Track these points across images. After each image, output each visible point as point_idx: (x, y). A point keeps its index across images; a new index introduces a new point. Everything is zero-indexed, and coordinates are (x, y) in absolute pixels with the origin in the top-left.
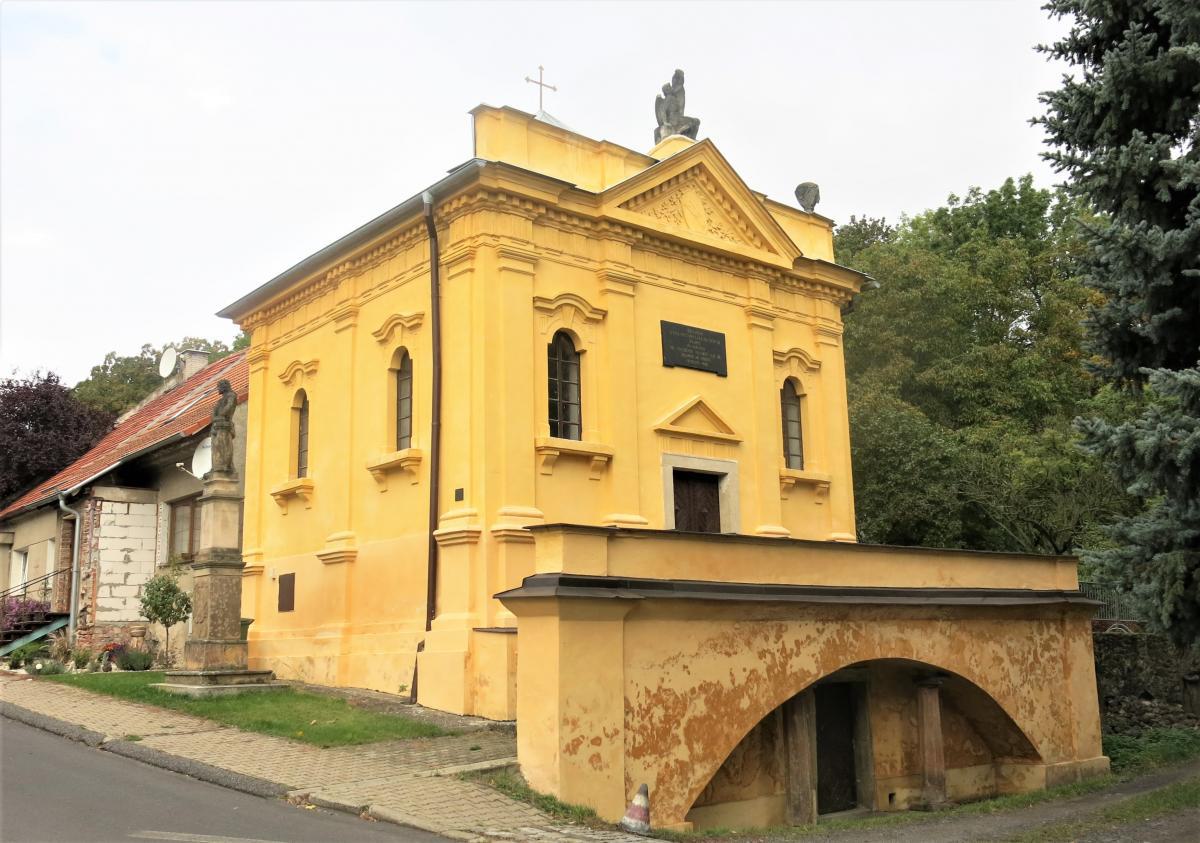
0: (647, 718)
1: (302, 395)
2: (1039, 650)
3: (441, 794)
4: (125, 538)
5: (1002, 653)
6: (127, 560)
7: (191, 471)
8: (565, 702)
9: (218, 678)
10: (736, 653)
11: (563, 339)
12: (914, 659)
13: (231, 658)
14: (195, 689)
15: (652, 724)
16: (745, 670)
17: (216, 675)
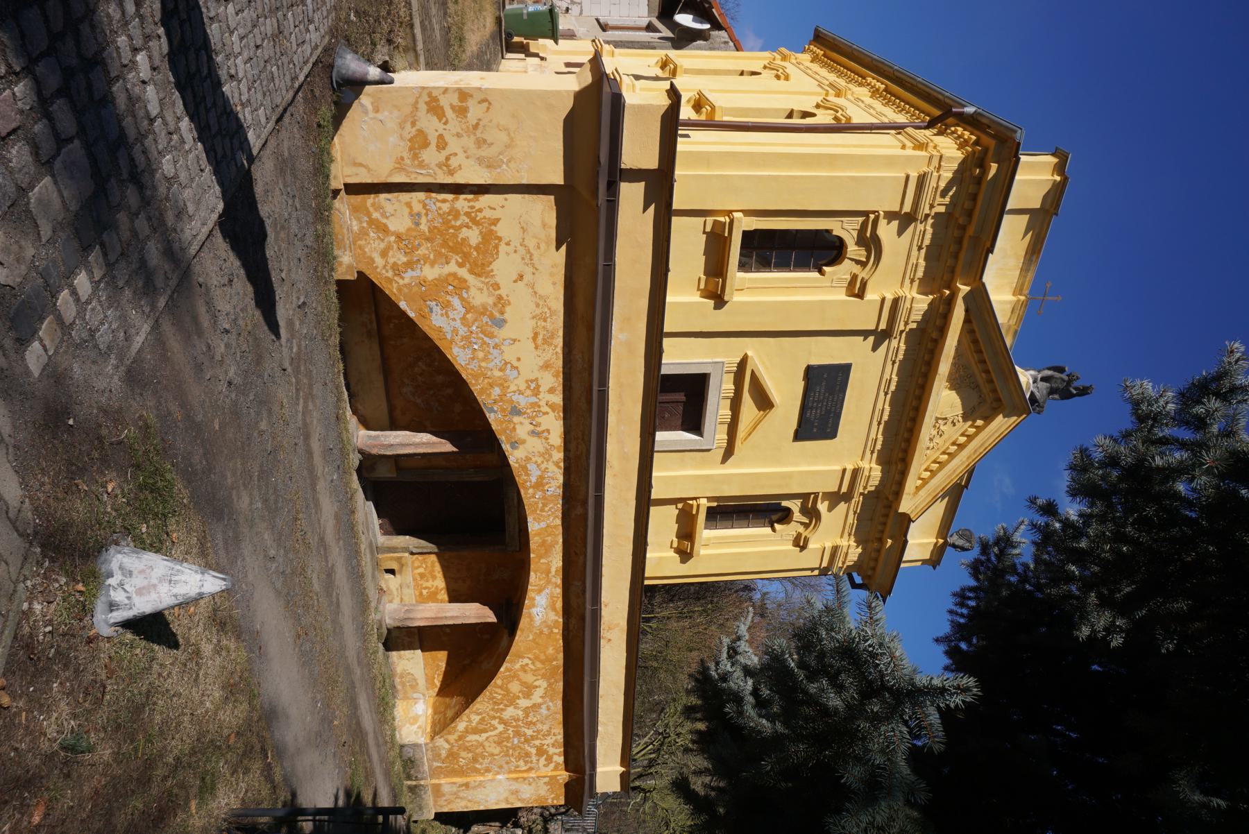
0: (467, 220)
2: (537, 742)
5: (537, 698)
7: (679, 13)
10: (536, 348)
11: (835, 252)
12: (530, 587)
15: (461, 227)
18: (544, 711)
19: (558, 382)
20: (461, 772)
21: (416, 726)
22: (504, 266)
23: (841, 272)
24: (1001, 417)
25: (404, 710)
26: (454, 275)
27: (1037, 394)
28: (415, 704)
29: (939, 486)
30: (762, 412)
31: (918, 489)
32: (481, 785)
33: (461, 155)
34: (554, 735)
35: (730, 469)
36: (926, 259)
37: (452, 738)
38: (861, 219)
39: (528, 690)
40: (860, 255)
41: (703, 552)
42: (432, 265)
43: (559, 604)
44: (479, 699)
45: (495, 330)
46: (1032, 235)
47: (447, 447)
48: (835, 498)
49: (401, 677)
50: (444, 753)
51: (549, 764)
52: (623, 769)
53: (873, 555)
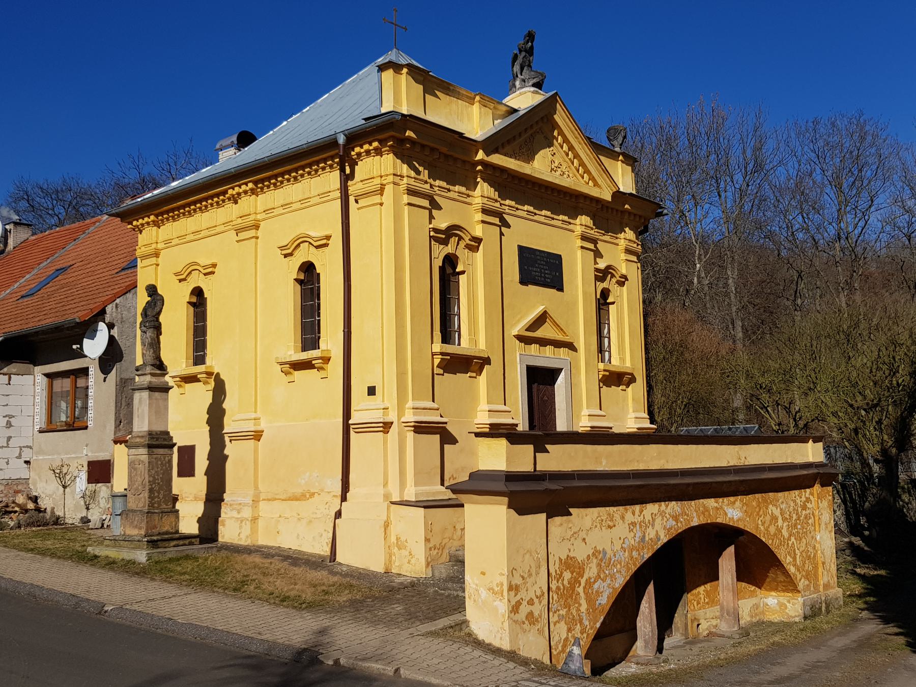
1: (198, 292)
2: (800, 510)
3: (346, 632)
4: (7, 405)
5: (777, 512)
6: (9, 425)
8: (512, 571)
9: (159, 543)
12: (724, 522)
13: (166, 525)
14: (141, 556)
16: (620, 538)
17: (158, 541)
18: (783, 506)
19: (630, 508)
20: (816, 568)
21: (788, 604)
22: (580, 553)
23: (463, 254)
24: (555, 117)
25: (774, 614)
26: (584, 588)
27: (535, 81)
28: (768, 605)
29: (596, 168)
30: (547, 320)
31: (596, 184)
32: (823, 553)
33: (536, 588)
34: (795, 497)
35: (581, 345)
36: (455, 186)
37: (799, 576)
38: (433, 242)
39: (774, 519)
40: (454, 241)
41: (628, 364)
42: (580, 605)
43: (732, 499)
44: (779, 557)
45: (608, 556)
46: (438, 91)
47: (651, 588)
48: (598, 254)
49: (752, 617)
50: (807, 582)
51: (810, 500)
52: (811, 441)
53: (632, 218)
